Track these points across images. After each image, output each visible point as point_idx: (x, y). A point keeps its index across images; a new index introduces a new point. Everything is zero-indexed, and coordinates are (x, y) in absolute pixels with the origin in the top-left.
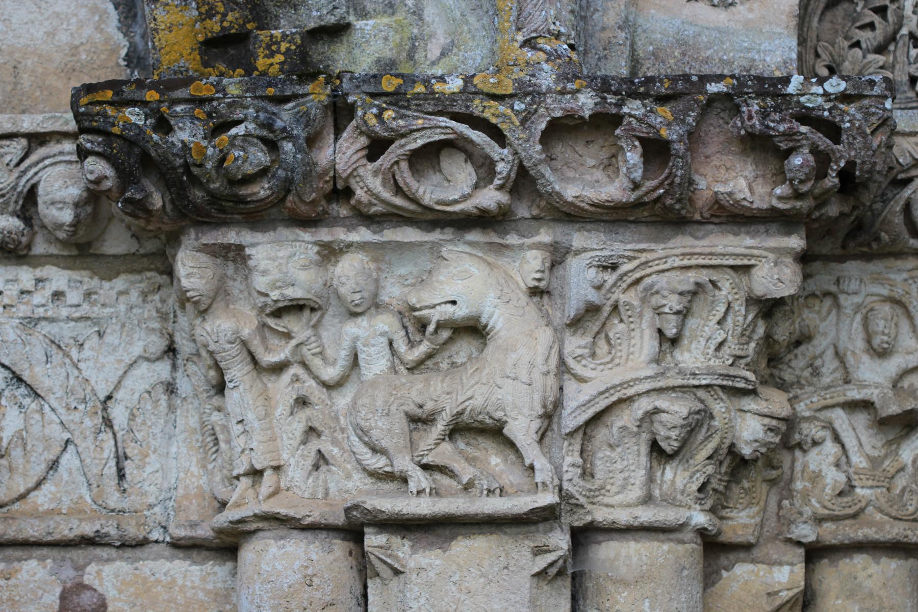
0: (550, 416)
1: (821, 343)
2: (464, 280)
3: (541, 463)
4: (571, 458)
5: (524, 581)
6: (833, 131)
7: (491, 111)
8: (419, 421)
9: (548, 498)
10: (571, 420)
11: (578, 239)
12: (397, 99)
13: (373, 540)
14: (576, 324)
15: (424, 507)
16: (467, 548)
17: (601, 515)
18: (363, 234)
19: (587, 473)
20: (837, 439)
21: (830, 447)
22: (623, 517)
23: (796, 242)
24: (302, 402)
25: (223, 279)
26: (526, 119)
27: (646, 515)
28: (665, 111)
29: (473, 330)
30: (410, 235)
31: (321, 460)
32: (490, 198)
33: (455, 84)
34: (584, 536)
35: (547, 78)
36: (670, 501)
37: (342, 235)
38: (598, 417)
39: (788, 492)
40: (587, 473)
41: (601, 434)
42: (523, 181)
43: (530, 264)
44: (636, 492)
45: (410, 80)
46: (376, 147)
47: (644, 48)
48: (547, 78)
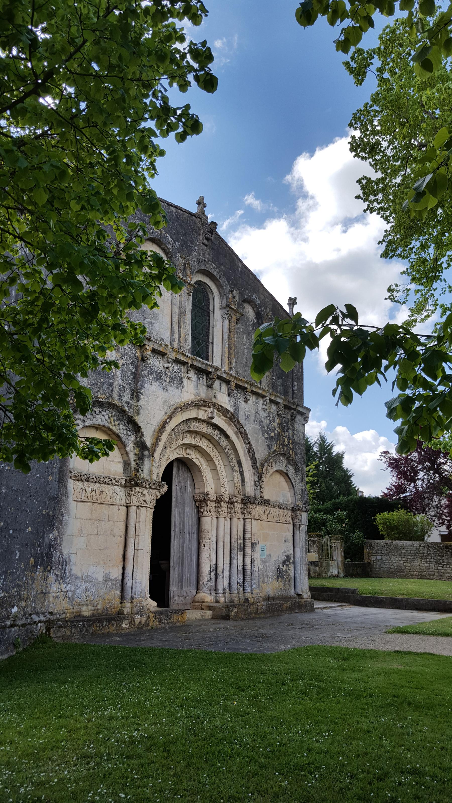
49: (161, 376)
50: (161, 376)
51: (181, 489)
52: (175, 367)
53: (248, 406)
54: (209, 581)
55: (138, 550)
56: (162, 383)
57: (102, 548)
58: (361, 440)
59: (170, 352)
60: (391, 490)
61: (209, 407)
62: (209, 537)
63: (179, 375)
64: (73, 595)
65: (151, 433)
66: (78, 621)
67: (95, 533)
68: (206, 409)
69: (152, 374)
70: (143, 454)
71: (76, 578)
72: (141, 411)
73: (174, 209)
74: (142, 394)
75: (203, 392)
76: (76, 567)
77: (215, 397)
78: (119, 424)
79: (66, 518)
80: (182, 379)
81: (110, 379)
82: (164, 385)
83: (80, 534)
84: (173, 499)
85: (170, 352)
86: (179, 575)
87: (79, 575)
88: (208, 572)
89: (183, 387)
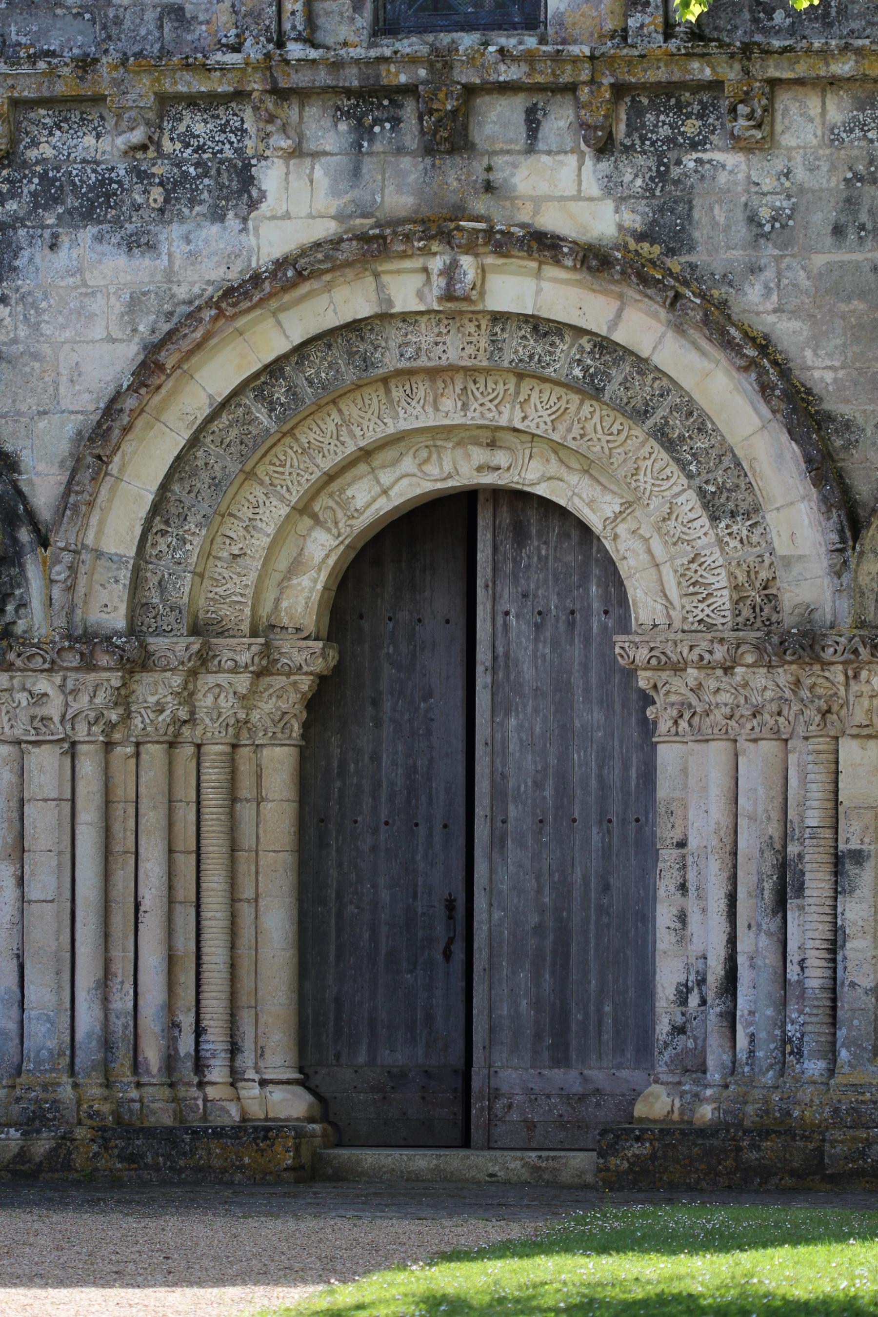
0: (63, 716)
1: (138, 692)
2: (43, 685)
3: (61, 728)
4: (68, 726)
5: (58, 755)
6: (124, 651)
7: (45, 647)
8: (33, 718)
9: (61, 736)
10: (69, 716)
11: (69, 674)
12: (23, 644)
13: (23, 746)
14: (70, 693)
15: (33, 738)
16: (44, 747)
17: (77, 739)
18: (19, 673)
19: (73, 729)
20: (142, 716)
21: (140, 719)
22: (82, 739)
23: (120, 674)
24: (8, 712)
25: (538, 285)
26: (53, 649)
27: (87, 739)
28: (85, 646)
29: (46, 695)
30: (30, 673)
31: (12, 726)
32: (47, 666)
33: (36, 640)
34: (74, 744)
35: (57, 639)
36: (94, 735)
37: (14, 674)
38: (75, 716)
39: (130, 729)
40: (73, 729)
41: (76, 720)
42: (53, 662)
43: (58, 680)
44: (85, 733)
45: (26, 639)
46: (19, 655)
47: (88, 624)
48: (57, 639)
49: (108, 196)
50: (108, 196)
51: (538, 627)
52: (199, 128)
53: (779, 165)
54: (679, 1030)
55: (29, 902)
56: (118, 223)
59: (117, 83)
62: (677, 836)
63: (229, 153)
65: (63, 447)
66: (240, 1184)
69: (57, 200)
70: (15, 541)
75: (399, 186)
77: (489, 187)
80: (248, 166)
82: (130, 228)
85: (117, 83)
86: (537, 1005)
89: (253, 205)
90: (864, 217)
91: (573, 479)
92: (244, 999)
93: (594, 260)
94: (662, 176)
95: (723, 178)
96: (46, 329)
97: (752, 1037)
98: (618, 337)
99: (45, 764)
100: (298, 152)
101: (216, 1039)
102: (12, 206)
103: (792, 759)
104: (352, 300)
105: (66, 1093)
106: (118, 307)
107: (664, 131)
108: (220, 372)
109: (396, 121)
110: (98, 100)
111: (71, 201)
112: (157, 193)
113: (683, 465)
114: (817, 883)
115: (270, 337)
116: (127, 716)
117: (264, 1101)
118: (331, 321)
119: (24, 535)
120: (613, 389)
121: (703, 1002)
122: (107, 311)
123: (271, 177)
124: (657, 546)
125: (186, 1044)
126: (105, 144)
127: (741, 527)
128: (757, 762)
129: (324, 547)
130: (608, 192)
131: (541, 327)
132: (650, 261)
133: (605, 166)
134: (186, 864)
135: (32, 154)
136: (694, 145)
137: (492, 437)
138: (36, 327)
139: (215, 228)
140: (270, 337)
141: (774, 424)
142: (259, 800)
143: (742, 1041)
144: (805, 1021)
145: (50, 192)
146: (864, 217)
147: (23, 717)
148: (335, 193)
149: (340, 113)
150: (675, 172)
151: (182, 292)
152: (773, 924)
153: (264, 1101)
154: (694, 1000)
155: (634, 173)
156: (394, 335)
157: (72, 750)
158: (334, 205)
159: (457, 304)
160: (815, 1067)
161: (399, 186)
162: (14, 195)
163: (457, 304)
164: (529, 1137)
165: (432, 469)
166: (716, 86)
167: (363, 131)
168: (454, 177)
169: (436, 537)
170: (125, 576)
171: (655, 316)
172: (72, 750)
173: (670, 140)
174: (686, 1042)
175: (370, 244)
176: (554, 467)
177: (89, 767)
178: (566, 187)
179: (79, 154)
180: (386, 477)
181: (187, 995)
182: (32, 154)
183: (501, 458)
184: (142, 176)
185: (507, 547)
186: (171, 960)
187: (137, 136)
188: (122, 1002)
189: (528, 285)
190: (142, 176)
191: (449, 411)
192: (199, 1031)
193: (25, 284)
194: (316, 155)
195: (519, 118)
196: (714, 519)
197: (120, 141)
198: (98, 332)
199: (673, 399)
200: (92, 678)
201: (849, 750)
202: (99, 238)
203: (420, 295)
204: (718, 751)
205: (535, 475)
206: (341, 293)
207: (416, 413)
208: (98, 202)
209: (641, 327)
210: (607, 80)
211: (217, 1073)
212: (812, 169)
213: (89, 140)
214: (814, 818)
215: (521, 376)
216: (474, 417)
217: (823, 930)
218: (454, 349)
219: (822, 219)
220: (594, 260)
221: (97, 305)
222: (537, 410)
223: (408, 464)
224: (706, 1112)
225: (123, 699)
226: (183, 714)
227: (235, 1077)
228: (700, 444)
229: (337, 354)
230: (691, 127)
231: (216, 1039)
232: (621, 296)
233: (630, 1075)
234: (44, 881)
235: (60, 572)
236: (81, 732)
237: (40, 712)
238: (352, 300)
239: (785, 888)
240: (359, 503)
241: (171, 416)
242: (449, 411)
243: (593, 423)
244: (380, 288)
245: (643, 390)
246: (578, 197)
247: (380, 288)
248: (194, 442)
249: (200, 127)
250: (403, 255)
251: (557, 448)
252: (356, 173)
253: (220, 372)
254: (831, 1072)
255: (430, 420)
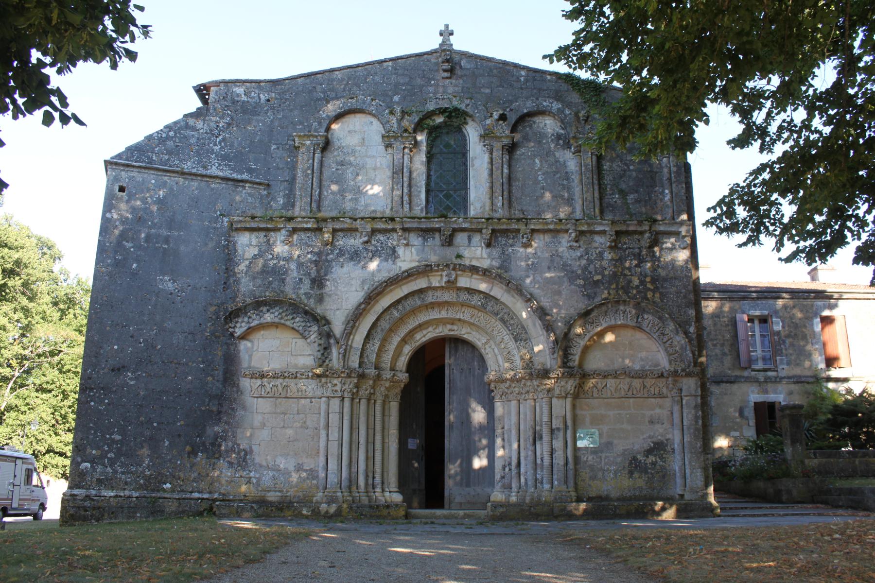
2: (335, 381)
52: (382, 238)
54: (503, 477)
57: (291, 439)
58: (737, 115)
60: (235, 281)
61: (443, 270)
64: (257, 482)
67: (282, 425)
68: (439, 273)
70: (329, 343)
71: (261, 466)
72: (326, 299)
73: (390, 63)
74: (328, 280)
76: (260, 457)
78: (250, 317)
79: (240, 413)
80: (394, 248)
81: (284, 274)
83: (263, 425)
84: (447, 386)
87: (264, 464)
88: (500, 467)
90: (555, 265)
91: (474, 333)
92: (385, 469)
93: (486, 273)
94: (503, 253)
95: (519, 254)
96: (340, 288)
97: (526, 480)
98: (492, 294)
99: (335, 404)
100: (407, 245)
101: (378, 480)
102: (331, 256)
103: (537, 404)
104: (421, 283)
105: (339, 494)
106: (359, 283)
107: (504, 242)
108: (386, 301)
109: (434, 238)
110: (356, 230)
111: (347, 255)
112: (370, 254)
113: (508, 328)
114: (546, 436)
115: (405, 289)
116: (358, 391)
117: (390, 497)
118: (416, 288)
119: (332, 341)
120: (489, 308)
121: (510, 470)
122: (356, 283)
123: (401, 251)
124: (496, 351)
125: (370, 481)
126: (357, 241)
127: (523, 343)
128: (526, 407)
129: (408, 350)
130: (489, 256)
131: (470, 291)
132: (499, 274)
133: (488, 250)
134: (371, 432)
135: (337, 243)
136: (511, 246)
137: (452, 321)
138: (336, 287)
139: (385, 264)
140: (405, 289)
141: (534, 317)
142: (390, 416)
143: (523, 480)
144: (541, 474)
145: (341, 253)
146: (555, 265)
147: (329, 389)
148: (418, 255)
149: (419, 236)
150: (507, 253)
151: (376, 279)
152: (533, 448)
153: (390, 497)
154: (507, 469)
155: (496, 252)
156: (430, 293)
157: (343, 399)
158: (417, 258)
159: (451, 285)
160: (547, 486)
161: (434, 252)
162: (332, 253)
163: (451, 285)
164: (461, 506)
165: (437, 331)
166: (518, 231)
167: (425, 240)
168: (450, 253)
169: (438, 345)
170: (359, 353)
171: (502, 288)
172: (343, 399)
173: (505, 244)
174: (506, 481)
175: (426, 270)
176: (469, 330)
177: (347, 403)
178: (476, 252)
179: (349, 244)
180: (425, 332)
181: (371, 467)
182: (337, 243)
183: (455, 327)
184: (366, 250)
185: (453, 352)
186: (367, 458)
187: (366, 239)
188: (354, 470)
189: (468, 279)
190: (366, 250)
191: (443, 314)
192: (374, 478)
193: (334, 276)
194: (413, 246)
195: (466, 238)
196: (516, 341)
197: (361, 241)
198: (354, 289)
199: (505, 311)
200: (349, 380)
201: (554, 401)
202: (354, 265)
203: (439, 282)
204: (514, 403)
205: (464, 332)
206: (418, 281)
207: (434, 315)
208: (355, 256)
209: (498, 292)
210: (491, 228)
211: (378, 489)
212: (542, 252)
213: (353, 240)
214: (545, 419)
215: (462, 306)
216: (450, 316)
217: (549, 450)
218: (447, 296)
219: (545, 264)
220: (486, 273)
221: (353, 282)
222: (465, 314)
223: (430, 329)
224: (514, 499)
225: (357, 386)
226: (372, 391)
227: (383, 491)
228: (512, 322)
229: (416, 298)
230: (511, 241)
231: (378, 480)
232: (493, 283)
233: (488, 490)
234: (334, 435)
235: (342, 351)
236: (346, 395)
237: (335, 388)
238: (421, 283)
239: (536, 437)
240: (418, 339)
241: (372, 312)
242: (443, 314)
243: (482, 318)
244: (429, 280)
245: (497, 308)
246: (482, 258)
247: (429, 280)
248: (378, 319)
249: (381, 237)
250: (437, 271)
251: (473, 324)
252: (423, 250)
253: (386, 301)
254: (552, 488)
255: (438, 316)
